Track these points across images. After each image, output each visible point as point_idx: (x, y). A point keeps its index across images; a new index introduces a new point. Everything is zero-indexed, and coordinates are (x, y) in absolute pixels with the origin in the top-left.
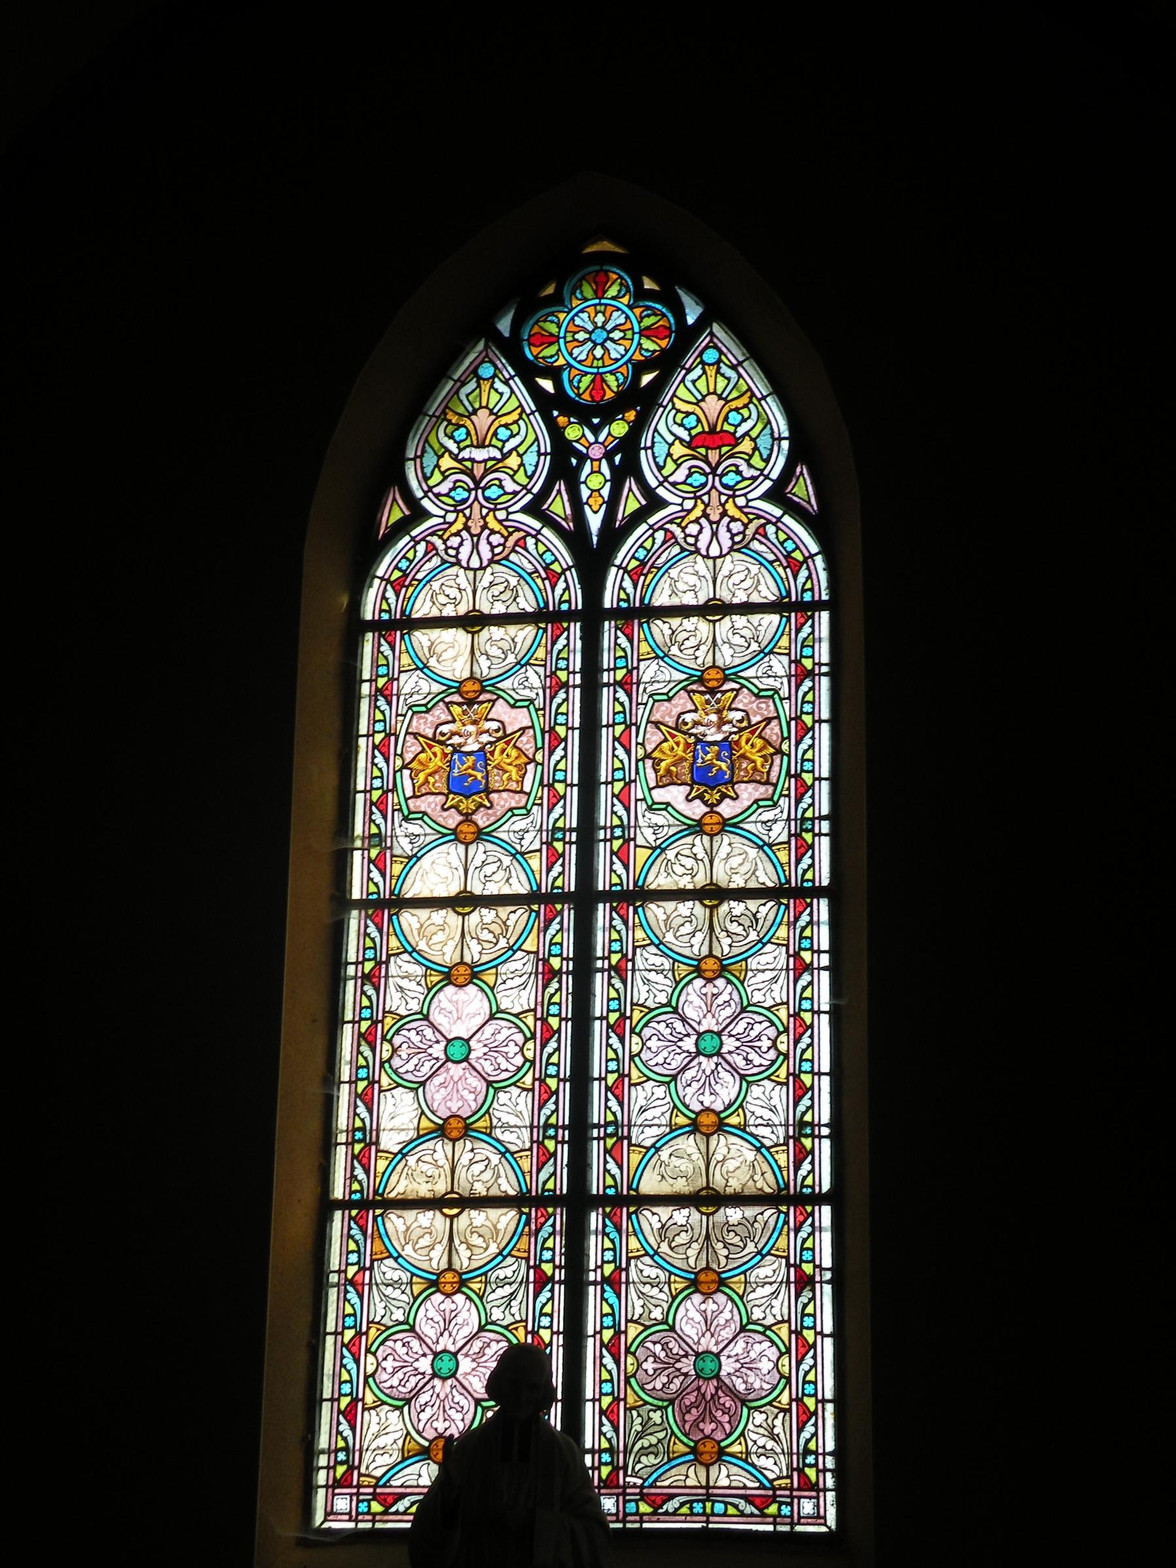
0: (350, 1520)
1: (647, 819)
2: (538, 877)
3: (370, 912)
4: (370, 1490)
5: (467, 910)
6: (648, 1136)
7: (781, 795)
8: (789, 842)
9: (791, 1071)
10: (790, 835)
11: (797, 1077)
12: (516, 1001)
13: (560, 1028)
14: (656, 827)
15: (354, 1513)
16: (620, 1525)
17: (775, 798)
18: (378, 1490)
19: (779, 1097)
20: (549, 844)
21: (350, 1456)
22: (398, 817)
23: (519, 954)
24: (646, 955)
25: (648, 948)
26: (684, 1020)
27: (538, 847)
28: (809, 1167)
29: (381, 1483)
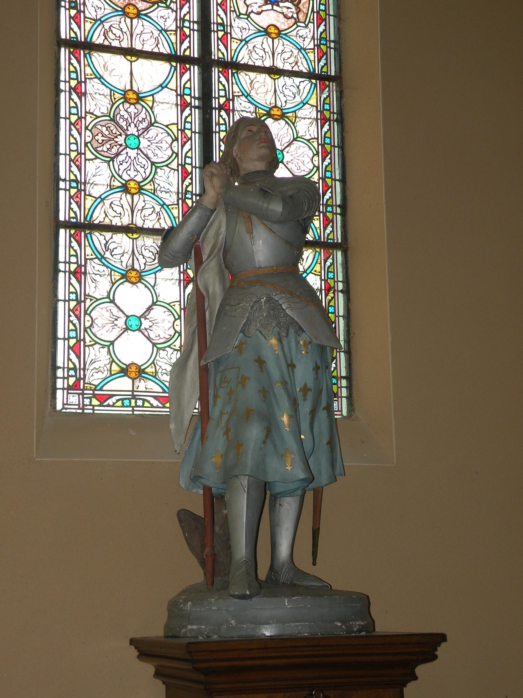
0: (79, 409)
1: (238, 23)
2: (175, 46)
3: (72, 50)
4: (91, 392)
5: (277, 77)
6: (96, 191)
7: (309, 22)
8: (314, 49)
9: (180, 163)
10: (315, 45)
11: (183, 167)
12: (307, 132)
13: (331, 150)
14: (242, 29)
15: (81, 405)
16: (80, 411)
17: (306, 23)
18: (96, 392)
19: (174, 177)
20: (318, 46)
21: (79, 372)
22: (234, 15)
23: (307, 106)
24: (241, 101)
25: (241, 97)
26: (147, 129)
27: (312, 47)
28: (331, 229)
29: (98, 388)
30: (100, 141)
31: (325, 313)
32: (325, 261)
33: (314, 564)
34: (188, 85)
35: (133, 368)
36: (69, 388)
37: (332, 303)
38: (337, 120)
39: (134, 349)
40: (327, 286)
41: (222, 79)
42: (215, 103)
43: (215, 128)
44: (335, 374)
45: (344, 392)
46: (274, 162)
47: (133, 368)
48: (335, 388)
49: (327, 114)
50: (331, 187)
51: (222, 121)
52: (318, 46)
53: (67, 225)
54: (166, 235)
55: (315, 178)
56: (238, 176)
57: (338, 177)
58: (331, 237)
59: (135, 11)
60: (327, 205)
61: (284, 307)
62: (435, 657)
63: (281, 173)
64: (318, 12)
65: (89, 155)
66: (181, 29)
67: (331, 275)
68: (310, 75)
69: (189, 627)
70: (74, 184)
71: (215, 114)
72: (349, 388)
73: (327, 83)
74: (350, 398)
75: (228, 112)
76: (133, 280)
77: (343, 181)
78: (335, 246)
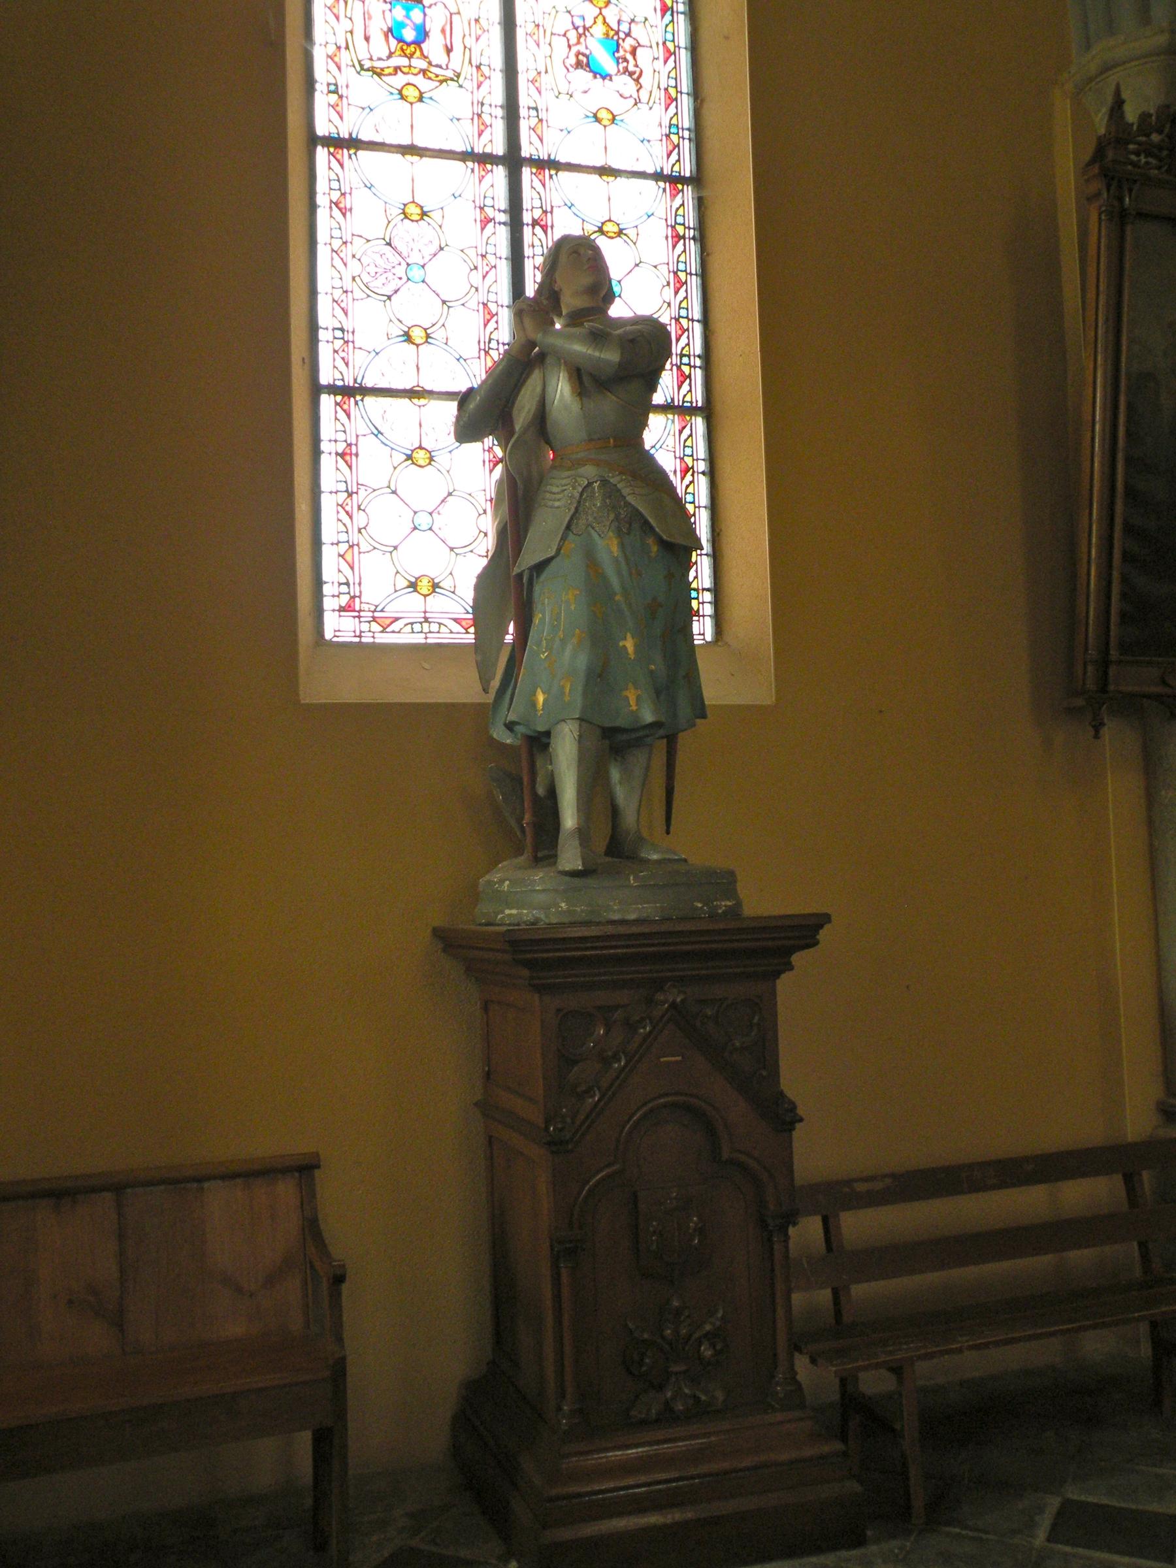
20: (668, 136)
29: (379, 609)
30: (373, 274)
31: (679, 503)
32: (681, 432)
33: (668, 832)
34: (489, 194)
35: (425, 581)
36: (342, 609)
37: (690, 490)
38: (694, 238)
39: (424, 557)
40: (684, 465)
41: (537, 184)
42: (527, 218)
43: (528, 251)
44: (694, 585)
45: (708, 609)
46: (610, 297)
47: (425, 581)
48: (694, 604)
49: (680, 229)
50: (688, 330)
51: (537, 243)
52: (668, 136)
53: (333, 389)
54: (464, 399)
55: (665, 319)
56: (560, 315)
57: (696, 318)
58: (688, 398)
59: (417, 94)
60: (682, 355)
61: (625, 492)
62: (816, 943)
63: (617, 310)
64: (666, 89)
65: (358, 294)
66: (479, 116)
67: (688, 451)
68: (658, 176)
69: (507, 912)
70: (339, 334)
71: (527, 231)
72: (716, 603)
73: (680, 186)
74: (718, 618)
75: (544, 228)
76: (421, 462)
77: (706, 321)
78: (692, 410)
